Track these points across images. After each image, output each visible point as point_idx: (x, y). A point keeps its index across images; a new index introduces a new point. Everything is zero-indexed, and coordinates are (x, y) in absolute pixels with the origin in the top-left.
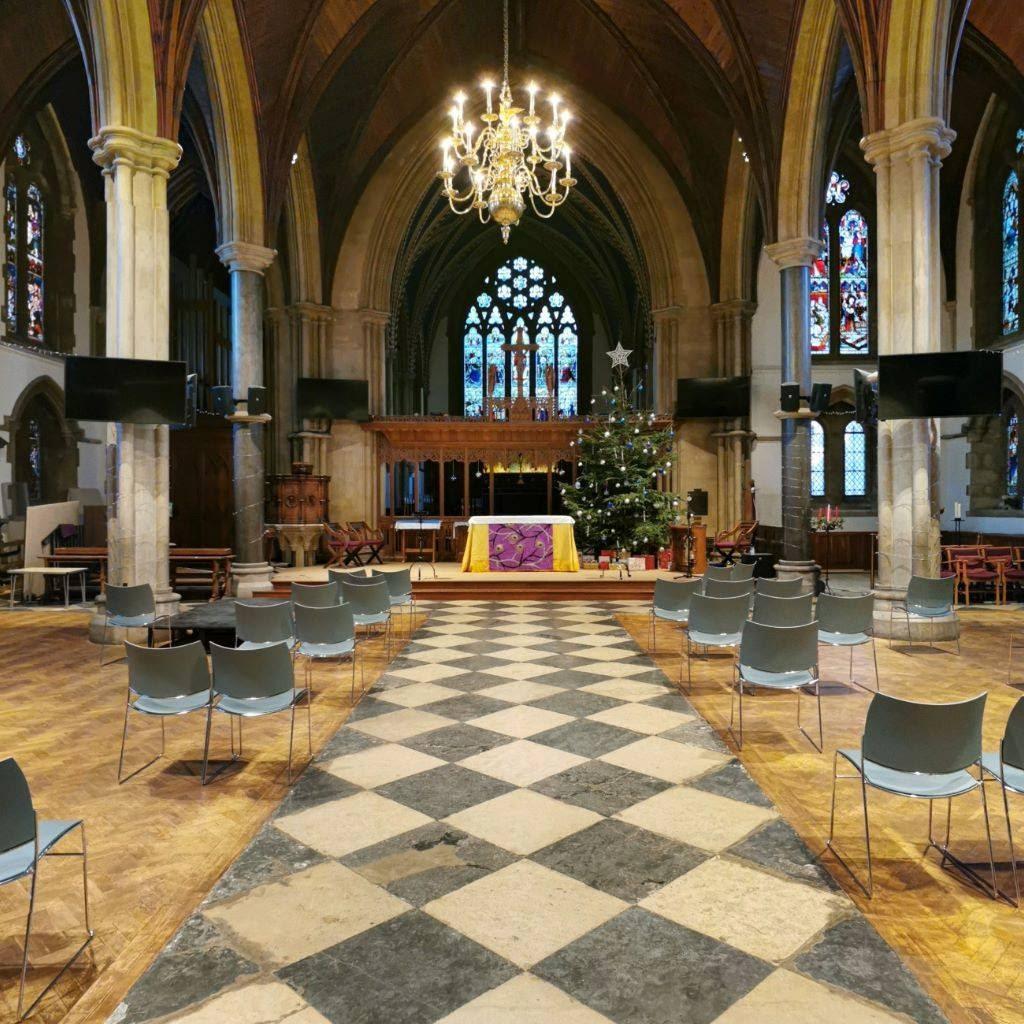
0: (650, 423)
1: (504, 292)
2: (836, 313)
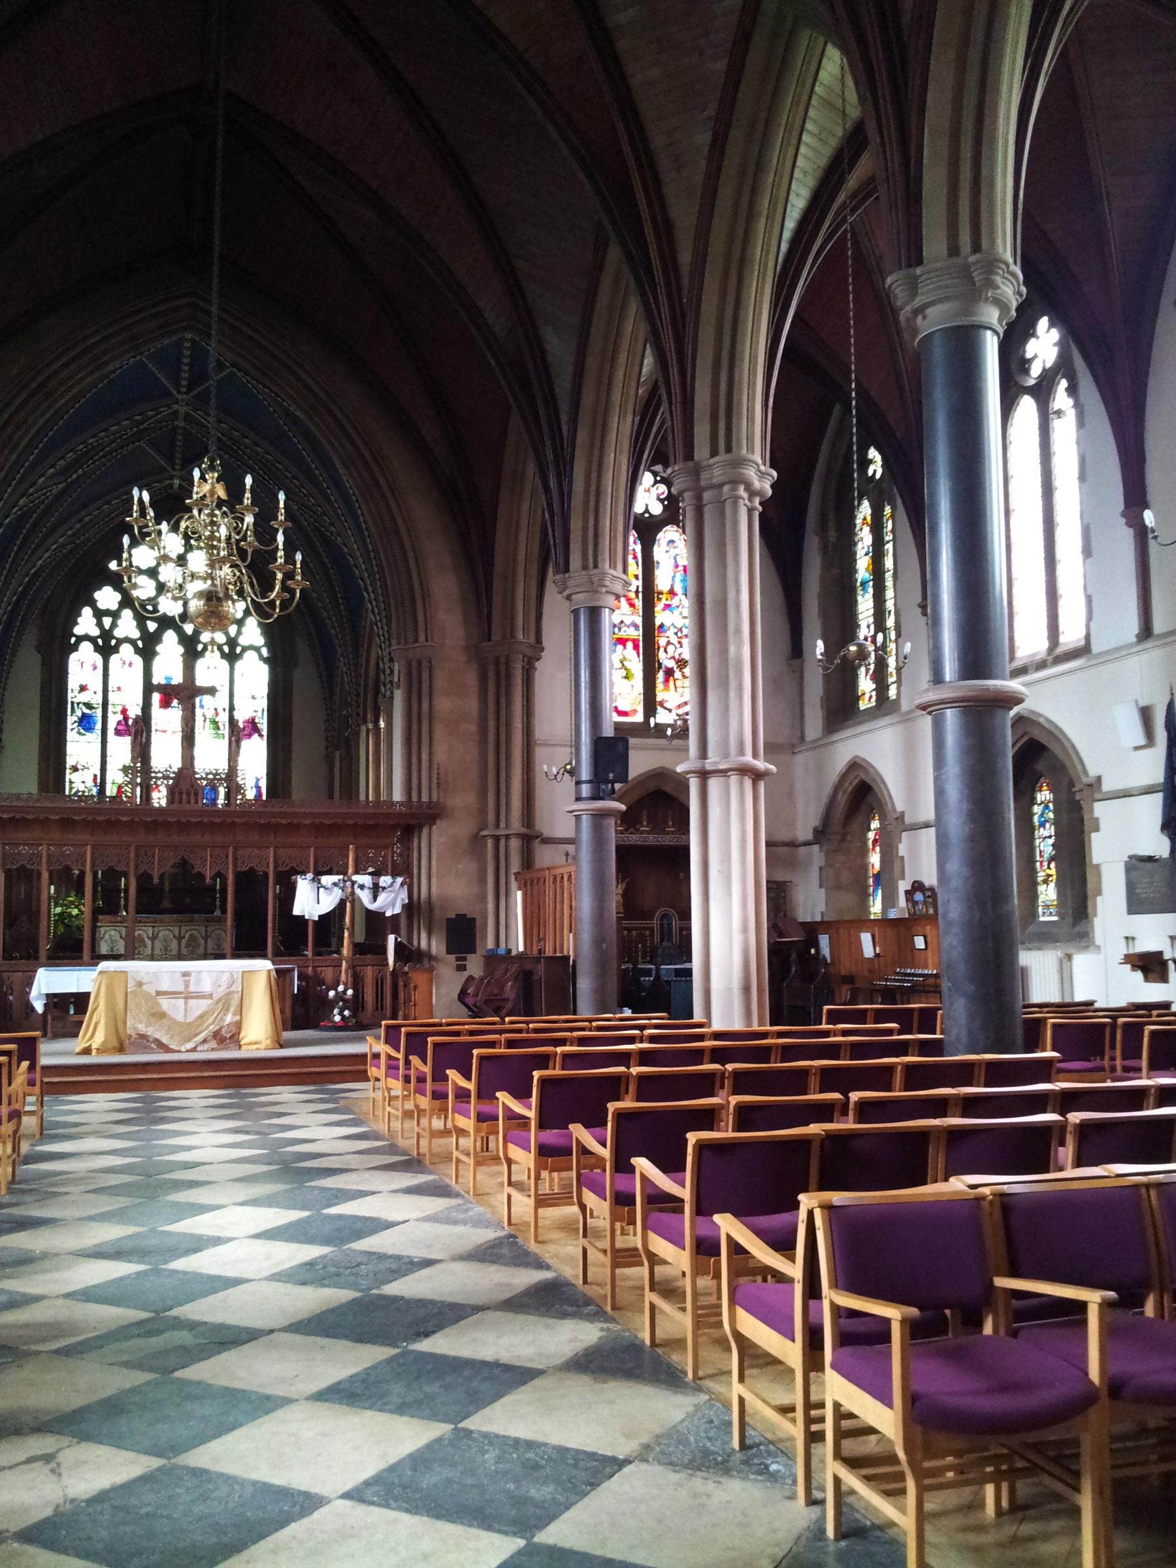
2: (651, 666)
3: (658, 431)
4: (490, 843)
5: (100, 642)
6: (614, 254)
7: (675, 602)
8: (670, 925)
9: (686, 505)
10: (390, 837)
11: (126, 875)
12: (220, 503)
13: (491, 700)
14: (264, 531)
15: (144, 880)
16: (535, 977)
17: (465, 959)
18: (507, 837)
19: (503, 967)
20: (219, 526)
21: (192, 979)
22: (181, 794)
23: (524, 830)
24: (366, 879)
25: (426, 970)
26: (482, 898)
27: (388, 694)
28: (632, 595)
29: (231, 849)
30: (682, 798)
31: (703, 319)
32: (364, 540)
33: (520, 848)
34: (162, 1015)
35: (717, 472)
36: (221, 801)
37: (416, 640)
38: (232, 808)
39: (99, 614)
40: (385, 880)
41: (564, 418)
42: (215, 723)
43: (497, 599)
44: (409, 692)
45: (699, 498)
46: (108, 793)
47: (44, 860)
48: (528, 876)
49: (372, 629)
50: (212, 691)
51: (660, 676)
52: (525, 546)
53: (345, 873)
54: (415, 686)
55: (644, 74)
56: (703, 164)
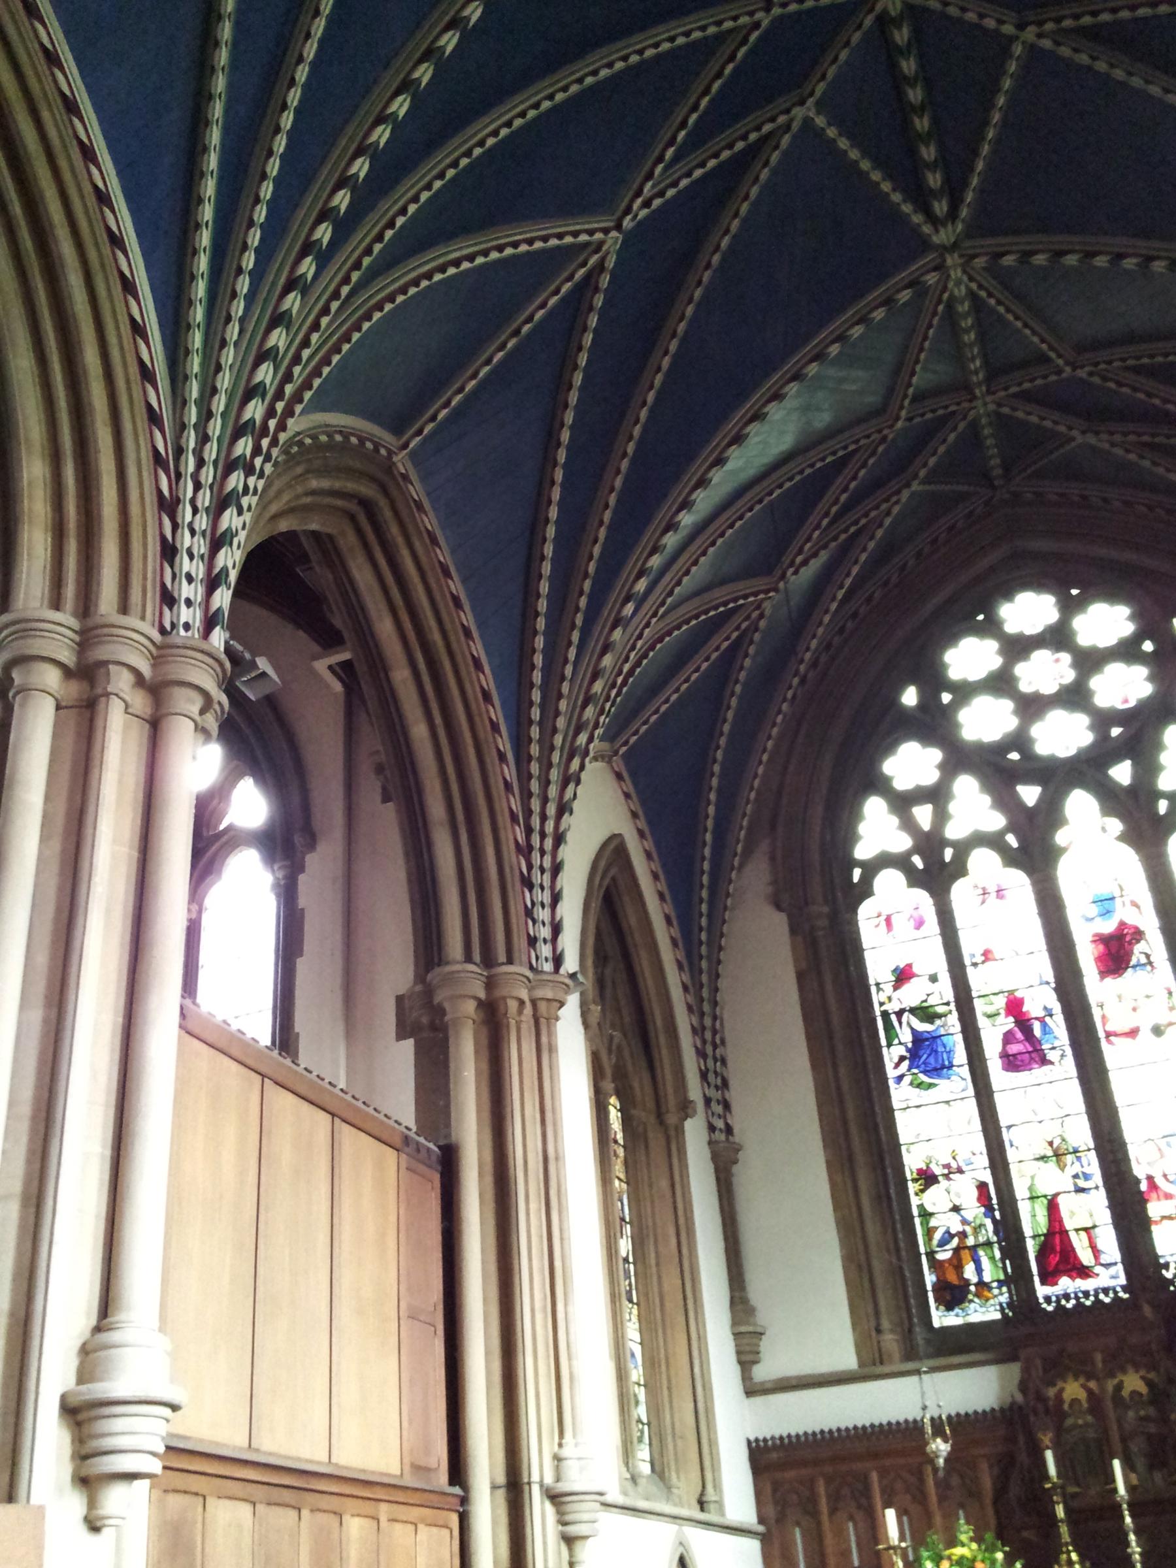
1: (984, 721)
39: (902, 803)
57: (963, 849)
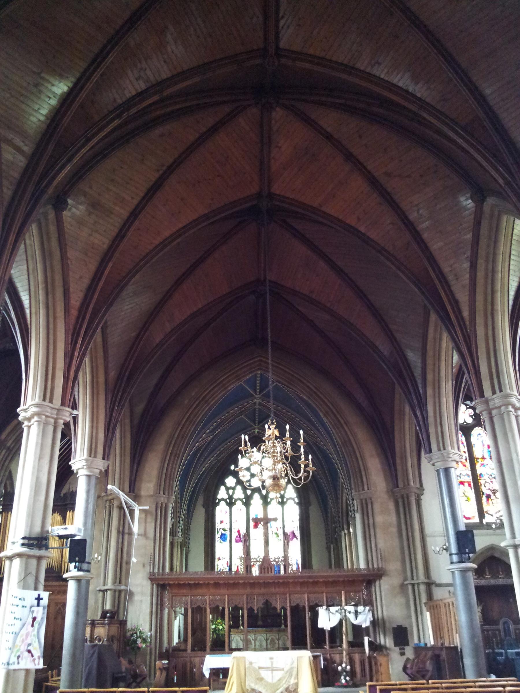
0: (132, 638)
3: (465, 386)
4: (410, 587)
5: (228, 501)
6: (433, 317)
7: (485, 462)
8: (509, 627)
9: (485, 417)
10: (361, 586)
11: (242, 609)
12: (276, 438)
13: (402, 516)
14: (295, 447)
15: (250, 610)
16: (441, 658)
17: (404, 649)
18: (418, 584)
19: (424, 653)
20: (276, 447)
21: (274, 660)
22: (264, 569)
23: (426, 581)
24: (351, 609)
25: (385, 655)
26: (410, 617)
27: (353, 516)
28: (464, 461)
29: (288, 595)
30: (505, 559)
31: (479, 337)
32: (335, 446)
33: (424, 590)
34: (261, 679)
35: (497, 401)
36: (282, 572)
37: (363, 490)
38: (287, 575)
39: (227, 489)
40: (360, 609)
41: (420, 386)
42: (277, 534)
43: (399, 468)
44: (363, 514)
45: (490, 413)
46: (233, 570)
47: (208, 602)
48: (431, 604)
49: (343, 486)
50: (275, 520)
51: (484, 499)
52: (409, 443)
53: (340, 605)
54: (365, 512)
55: (436, 246)
56: (468, 276)
57: (236, 500)
